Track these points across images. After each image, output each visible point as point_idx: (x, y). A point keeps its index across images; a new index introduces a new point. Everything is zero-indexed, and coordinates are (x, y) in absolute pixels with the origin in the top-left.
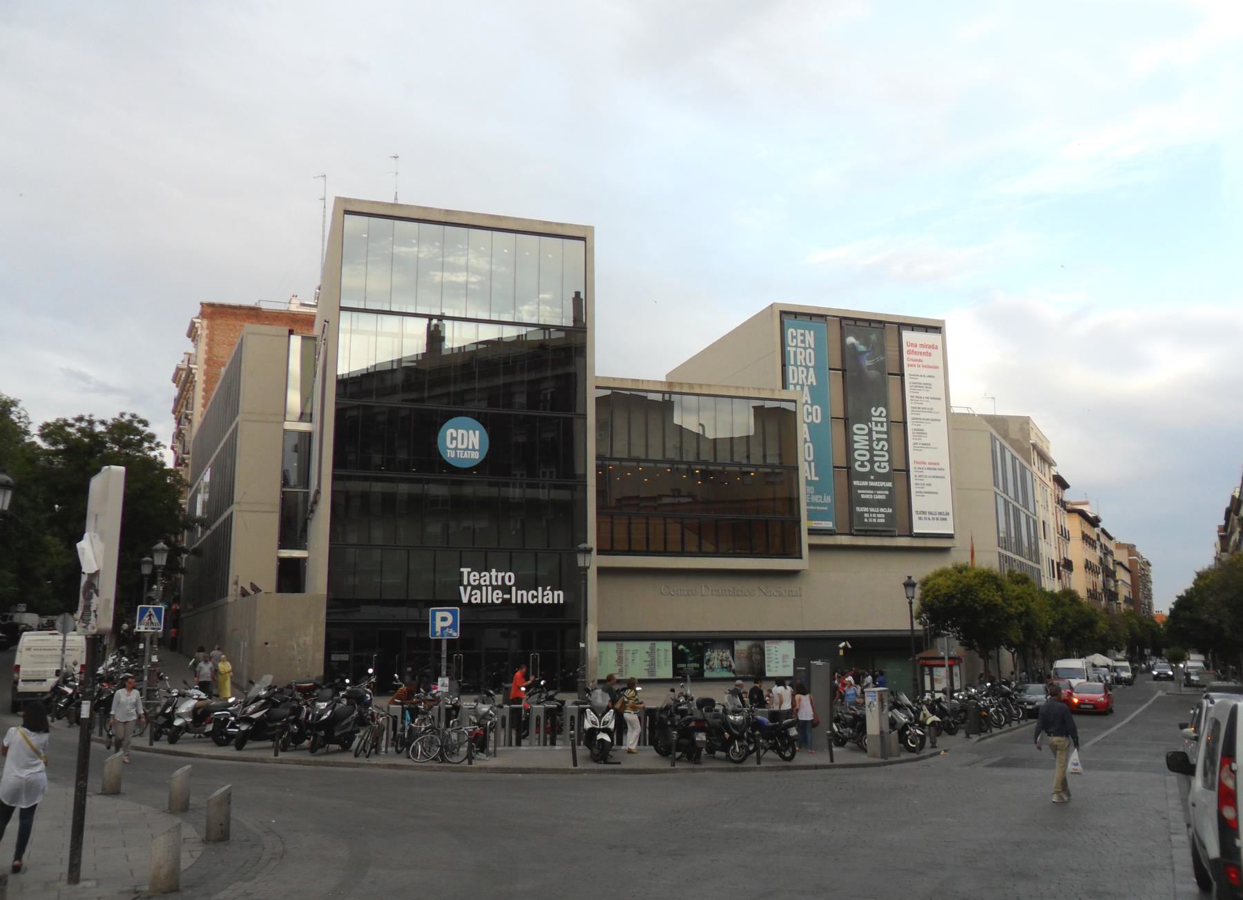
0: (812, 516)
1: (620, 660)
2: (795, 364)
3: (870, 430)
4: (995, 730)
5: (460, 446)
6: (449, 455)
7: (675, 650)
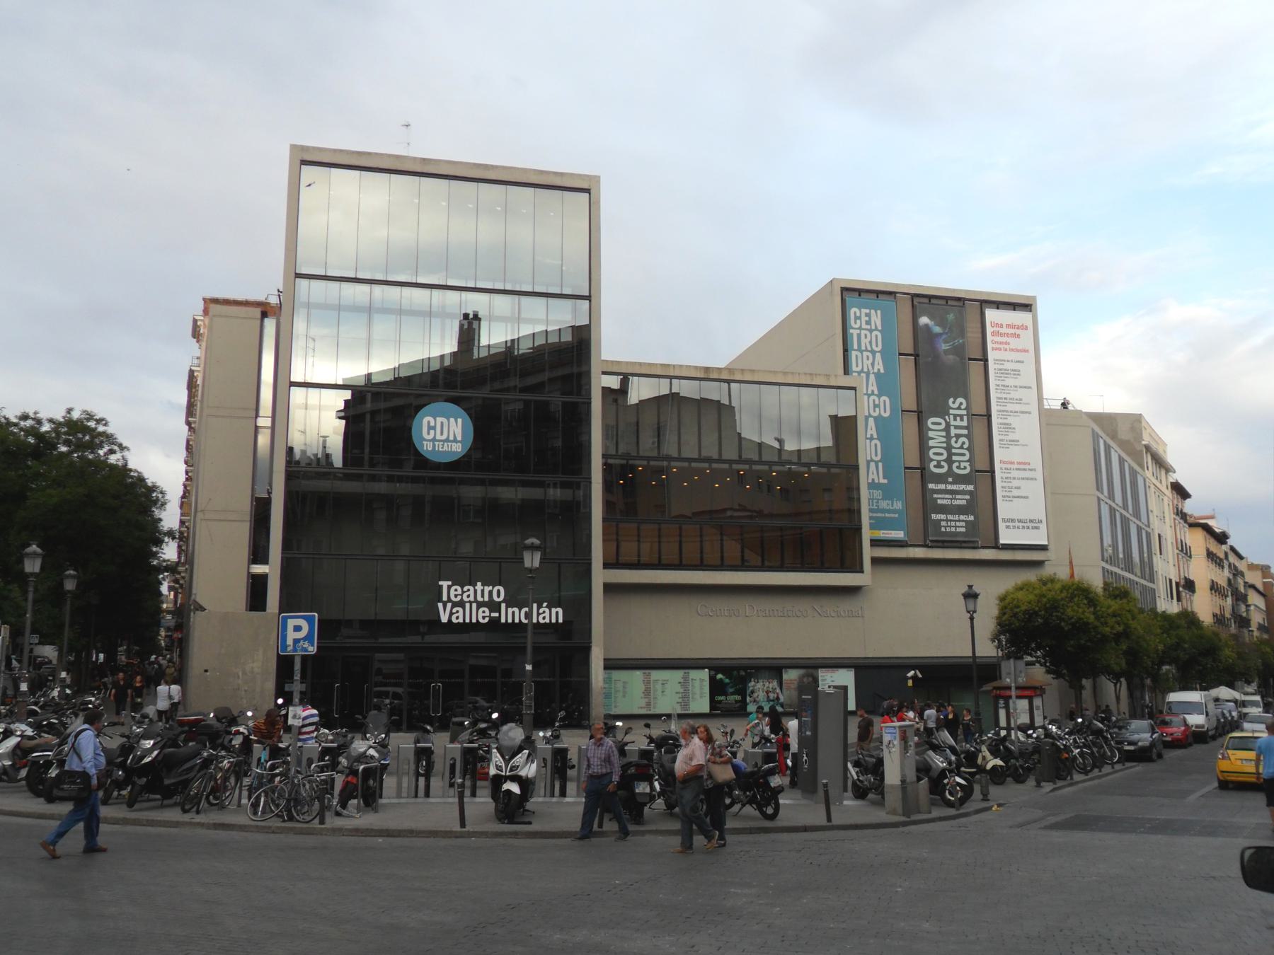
0: (877, 524)
1: (647, 692)
2: (859, 349)
3: (948, 425)
4: (1077, 777)
5: (438, 437)
6: (426, 448)
7: (712, 680)
